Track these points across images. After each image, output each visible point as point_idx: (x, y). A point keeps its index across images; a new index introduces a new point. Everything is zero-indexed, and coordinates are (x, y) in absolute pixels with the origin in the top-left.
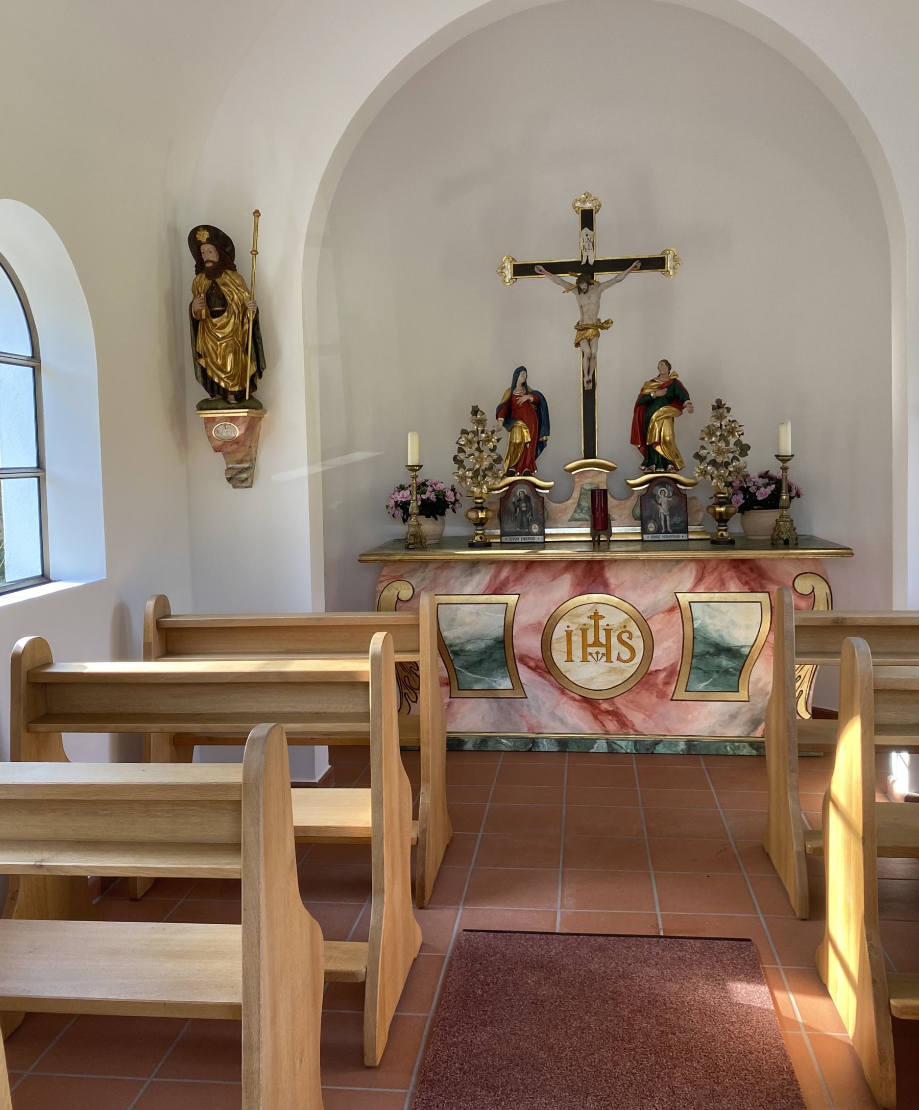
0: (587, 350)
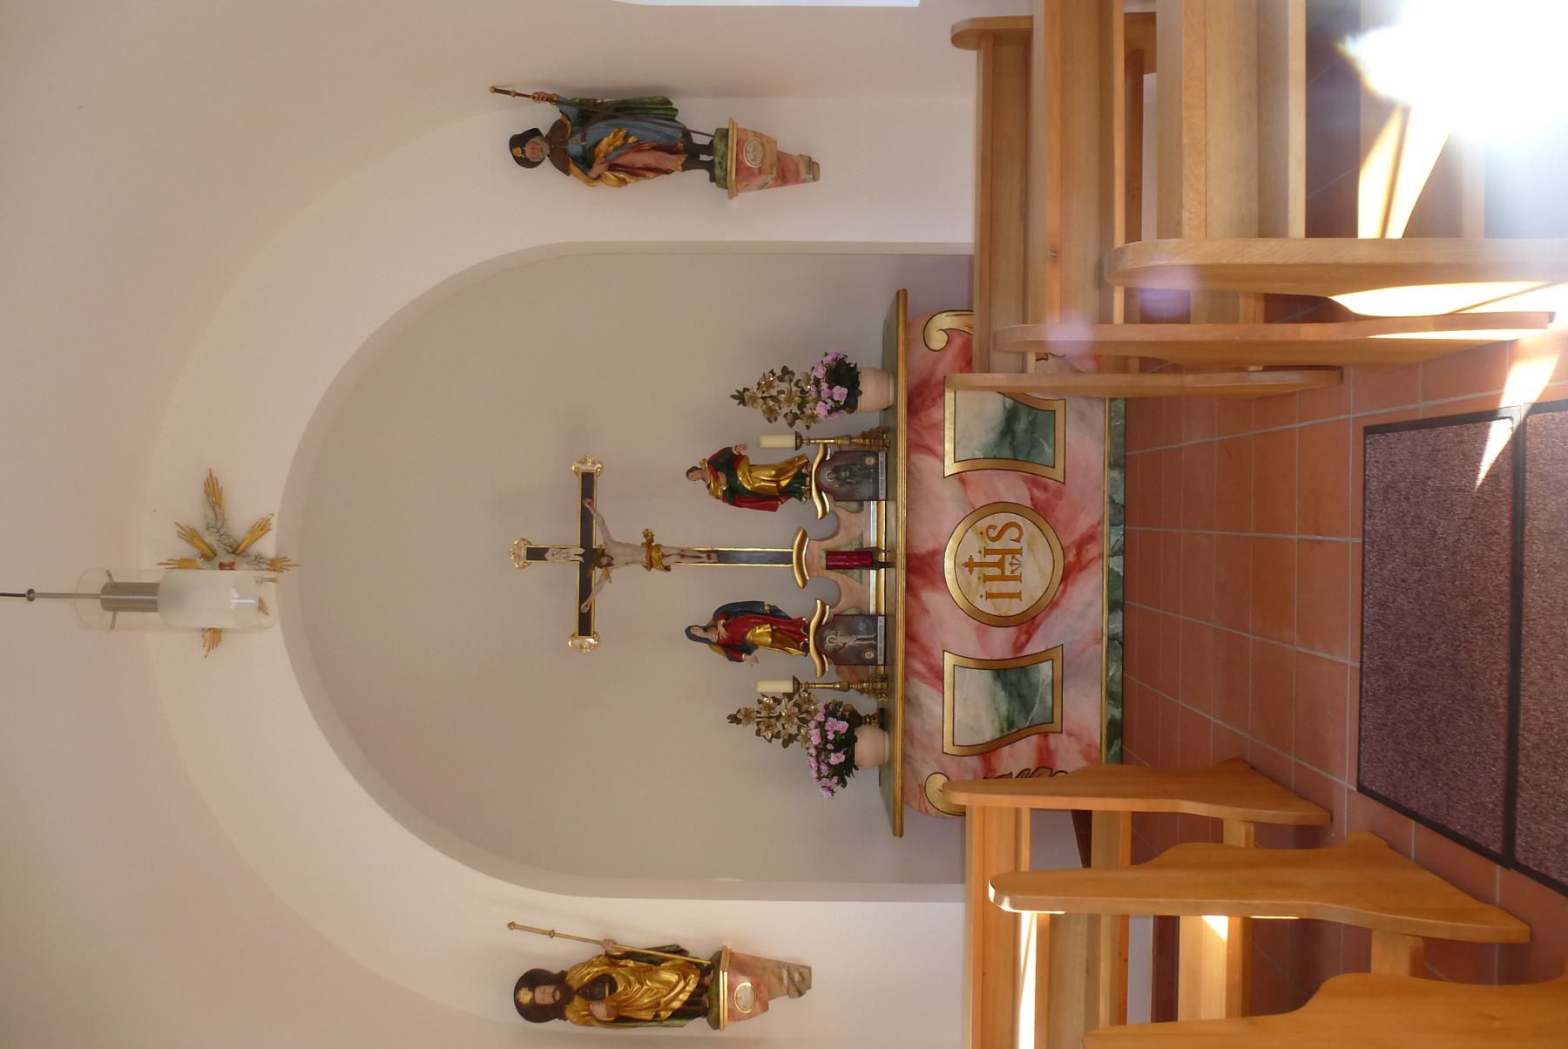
0: (674, 558)
